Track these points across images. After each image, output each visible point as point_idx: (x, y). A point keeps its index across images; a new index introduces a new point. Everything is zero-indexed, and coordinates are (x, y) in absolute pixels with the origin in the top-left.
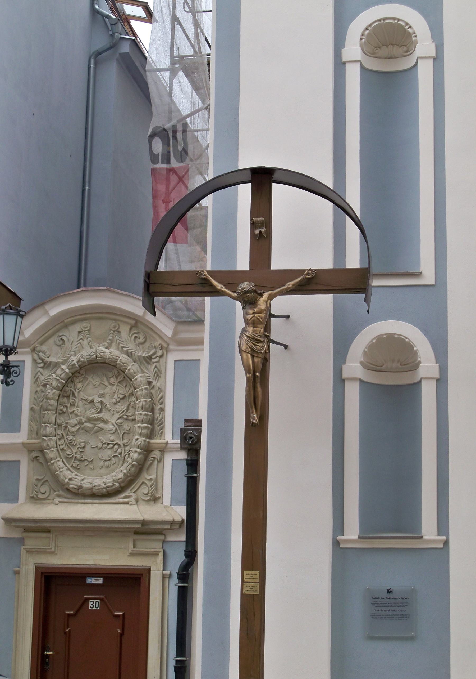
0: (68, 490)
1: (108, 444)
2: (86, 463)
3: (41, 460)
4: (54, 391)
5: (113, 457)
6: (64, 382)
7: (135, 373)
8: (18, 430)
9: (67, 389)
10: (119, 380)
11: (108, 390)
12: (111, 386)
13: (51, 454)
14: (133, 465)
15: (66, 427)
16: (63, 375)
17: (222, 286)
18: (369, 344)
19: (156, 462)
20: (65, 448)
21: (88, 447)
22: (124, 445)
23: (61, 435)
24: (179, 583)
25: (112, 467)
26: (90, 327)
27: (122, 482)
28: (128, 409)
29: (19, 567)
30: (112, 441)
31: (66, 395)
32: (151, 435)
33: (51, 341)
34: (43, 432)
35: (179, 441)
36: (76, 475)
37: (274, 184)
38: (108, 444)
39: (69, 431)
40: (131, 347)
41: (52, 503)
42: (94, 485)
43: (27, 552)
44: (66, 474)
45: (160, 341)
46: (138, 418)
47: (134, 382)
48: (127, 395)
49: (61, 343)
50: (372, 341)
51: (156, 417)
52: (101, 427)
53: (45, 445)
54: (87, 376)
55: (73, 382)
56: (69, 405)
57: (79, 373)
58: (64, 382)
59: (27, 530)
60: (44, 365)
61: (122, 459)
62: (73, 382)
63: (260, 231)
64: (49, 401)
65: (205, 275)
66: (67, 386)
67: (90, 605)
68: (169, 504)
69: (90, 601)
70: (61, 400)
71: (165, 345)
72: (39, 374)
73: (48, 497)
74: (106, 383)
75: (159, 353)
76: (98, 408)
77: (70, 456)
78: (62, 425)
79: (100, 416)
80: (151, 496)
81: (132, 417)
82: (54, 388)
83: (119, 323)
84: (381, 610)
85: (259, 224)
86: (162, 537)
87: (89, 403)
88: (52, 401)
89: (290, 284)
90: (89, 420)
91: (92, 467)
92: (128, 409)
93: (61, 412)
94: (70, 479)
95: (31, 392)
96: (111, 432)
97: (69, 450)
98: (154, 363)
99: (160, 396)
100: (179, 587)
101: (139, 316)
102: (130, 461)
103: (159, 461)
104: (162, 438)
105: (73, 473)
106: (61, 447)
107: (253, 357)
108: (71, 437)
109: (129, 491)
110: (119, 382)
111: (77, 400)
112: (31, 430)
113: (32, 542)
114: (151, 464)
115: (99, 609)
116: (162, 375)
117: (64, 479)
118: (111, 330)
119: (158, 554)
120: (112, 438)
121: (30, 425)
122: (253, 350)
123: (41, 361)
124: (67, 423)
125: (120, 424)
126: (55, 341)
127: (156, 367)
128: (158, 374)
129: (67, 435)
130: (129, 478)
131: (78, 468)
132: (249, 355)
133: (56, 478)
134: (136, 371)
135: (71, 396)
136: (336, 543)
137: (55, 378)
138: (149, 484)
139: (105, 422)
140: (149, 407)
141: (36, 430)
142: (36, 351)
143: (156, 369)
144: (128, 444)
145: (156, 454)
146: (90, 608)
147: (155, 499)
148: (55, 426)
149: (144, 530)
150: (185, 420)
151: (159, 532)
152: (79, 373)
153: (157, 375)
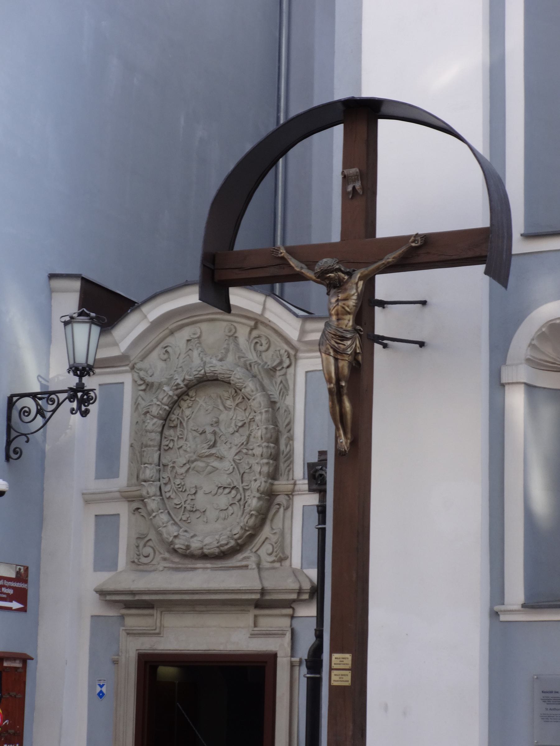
0: (175, 551)
1: (225, 488)
2: (198, 514)
4: (155, 420)
5: (231, 505)
6: (167, 408)
7: (252, 391)
8: (116, 475)
9: (173, 417)
10: (237, 402)
12: (226, 412)
13: (152, 504)
14: (252, 515)
16: (166, 399)
17: (304, 266)
18: (537, 332)
19: (282, 510)
20: (172, 497)
21: (200, 494)
22: (244, 489)
23: (167, 479)
26: (201, 332)
27: (240, 538)
29: (118, 655)
30: (230, 485)
31: (172, 425)
32: (274, 475)
33: (155, 355)
34: (142, 477)
35: (306, 481)
37: (381, 123)
38: (225, 488)
39: (176, 473)
42: (204, 544)
43: (128, 634)
49: (165, 357)
50: (540, 329)
52: (215, 466)
53: (144, 493)
54: (197, 399)
55: (180, 407)
56: (176, 439)
57: (188, 395)
58: (167, 408)
59: (128, 605)
60: (147, 387)
61: (242, 507)
63: (354, 188)
64: (148, 433)
65: (281, 253)
66: (173, 414)
68: (299, 567)
71: (292, 352)
72: (140, 399)
73: (152, 561)
74: (221, 407)
75: (286, 363)
76: (210, 441)
77: (178, 507)
78: (168, 465)
79: (213, 451)
80: (276, 556)
82: (154, 417)
83: (235, 324)
84: (555, 709)
85: (352, 177)
86: (289, 611)
87: (201, 434)
88: (153, 434)
89: (390, 258)
90: (201, 457)
93: (167, 448)
94: (176, 537)
95: (131, 423)
96: (228, 472)
100: (308, 678)
101: (354, 316)
103: (286, 509)
105: (181, 528)
106: (168, 495)
107: (336, 360)
108: (178, 481)
109: (249, 551)
110: (237, 405)
111: (185, 432)
112: (130, 474)
113: (135, 621)
114: (277, 512)
116: (291, 393)
119: (285, 635)
123: (142, 382)
124: (174, 462)
125: (238, 461)
128: (285, 389)
129: (175, 478)
130: (248, 533)
131: (189, 521)
135: (179, 425)
136: (494, 615)
137: (156, 404)
139: (221, 458)
140: (272, 436)
142: (137, 369)
143: (281, 385)
145: (281, 499)
148: (158, 467)
149: (263, 602)
152: (188, 395)
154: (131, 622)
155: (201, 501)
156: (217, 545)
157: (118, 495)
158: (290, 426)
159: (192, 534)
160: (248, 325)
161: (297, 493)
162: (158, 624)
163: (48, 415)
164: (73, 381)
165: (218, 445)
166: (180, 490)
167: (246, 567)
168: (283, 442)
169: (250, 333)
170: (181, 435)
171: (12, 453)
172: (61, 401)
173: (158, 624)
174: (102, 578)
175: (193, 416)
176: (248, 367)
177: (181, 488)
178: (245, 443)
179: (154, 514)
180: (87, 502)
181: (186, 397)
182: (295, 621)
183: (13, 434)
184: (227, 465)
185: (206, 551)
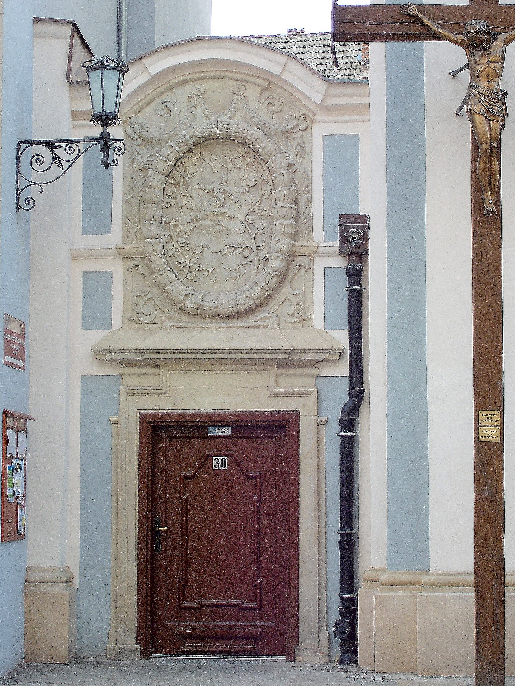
2: (206, 273)
3: (143, 269)
4: (161, 176)
7: (272, 152)
9: (176, 174)
11: (233, 175)
13: (158, 262)
15: (176, 226)
16: (172, 154)
21: (207, 253)
24: (342, 431)
25: (242, 279)
27: (258, 299)
28: (261, 201)
29: (118, 415)
32: (295, 236)
33: (150, 109)
35: (337, 244)
36: (194, 290)
40: (264, 117)
41: (161, 328)
42: (219, 303)
44: (178, 290)
45: (303, 110)
46: (276, 213)
47: (272, 165)
48: (259, 182)
49: (165, 111)
51: (301, 211)
55: (183, 165)
57: (192, 152)
59: (124, 364)
61: (256, 268)
62: (183, 165)
65: (413, 11)
67: (215, 463)
68: (322, 327)
69: (214, 458)
70: (169, 189)
74: (230, 167)
75: (303, 126)
79: (224, 210)
81: (268, 212)
83: (244, 83)
86: (314, 371)
90: (208, 216)
91: (213, 279)
92: (261, 201)
94: (186, 295)
96: (238, 232)
97: (181, 257)
98: (295, 138)
99: (306, 183)
102: (270, 271)
104: (311, 239)
106: (170, 253)
108: (182, 240)
111: (190, 189)
112: (126, 231)
113: (137, 379)
115: (226, 468)
117: (178, 295)
118: (235, 94)
120: (240, 240)
121: (125, 224)
122: (490, 112)
125: (250, 222)
126: (156, 110)
127: (298, 144)
128: (303, 152)
129: (178, 236)
132: (484, 119)
133: (167, 295)
134: (273, 149)
135: (182, 182)
138: (295, 300)
139: (231, 218)
141: (134, 230)
143: (299, 147)
144: (263, 247)
145: (302, 260)
146: (214, 468)
147: (304, 320)
149: (289, 362)
150: (341, 216)
151: (311, 364)
153: (301, 155)
154: (130, 382)
155: (208, 260)
156: (235, 305)
157: (114, 251)
158: (308, 189)
159: (203, 293)
160: (259, 85)
161: (319, 255)
162: (164, 384)
163: (66, 165)
164: (97, 131)
165: (227, 204)
166: (185, 248)
167: (266, 327)
168: (302, 203)
169: (261, 94)
170: (185, 192)
171: (21, 203)
172: (81, 152)
173: (164, 384)
174: (96, 337)
175: (198, 174)
176: (262, 127)
177: (185, 248)
178: (257, 204)
179: (161, 272)
180: (74, 257)
181: (190, 155)
182: (318, 379)
183: (23, 183)
184: (237, 225)
185: (220, 311)
